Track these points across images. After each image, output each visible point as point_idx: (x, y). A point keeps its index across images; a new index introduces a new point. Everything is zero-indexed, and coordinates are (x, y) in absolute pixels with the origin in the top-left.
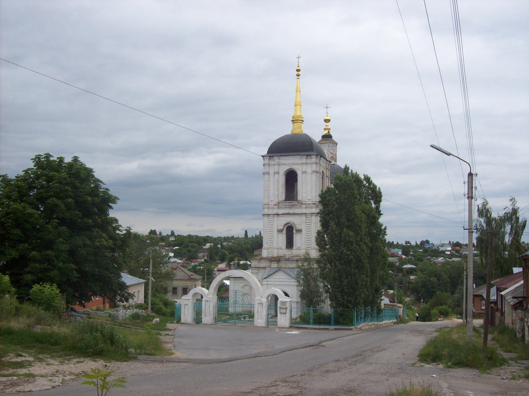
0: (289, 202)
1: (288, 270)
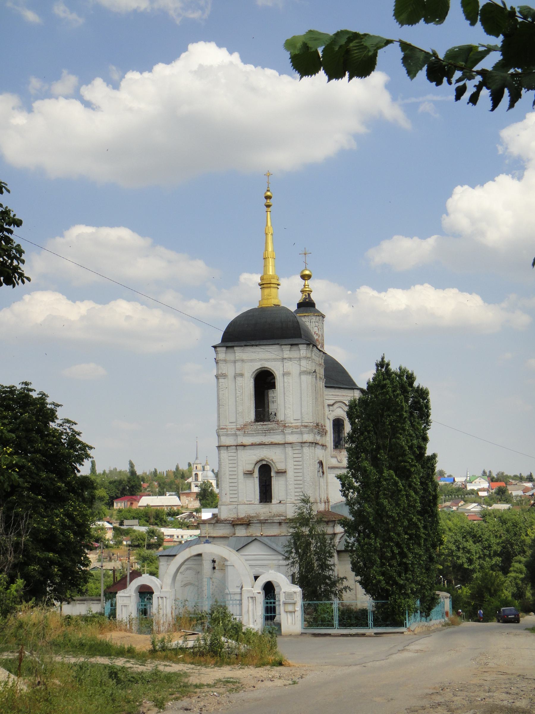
0: (262, 423)
1: (267, 541)
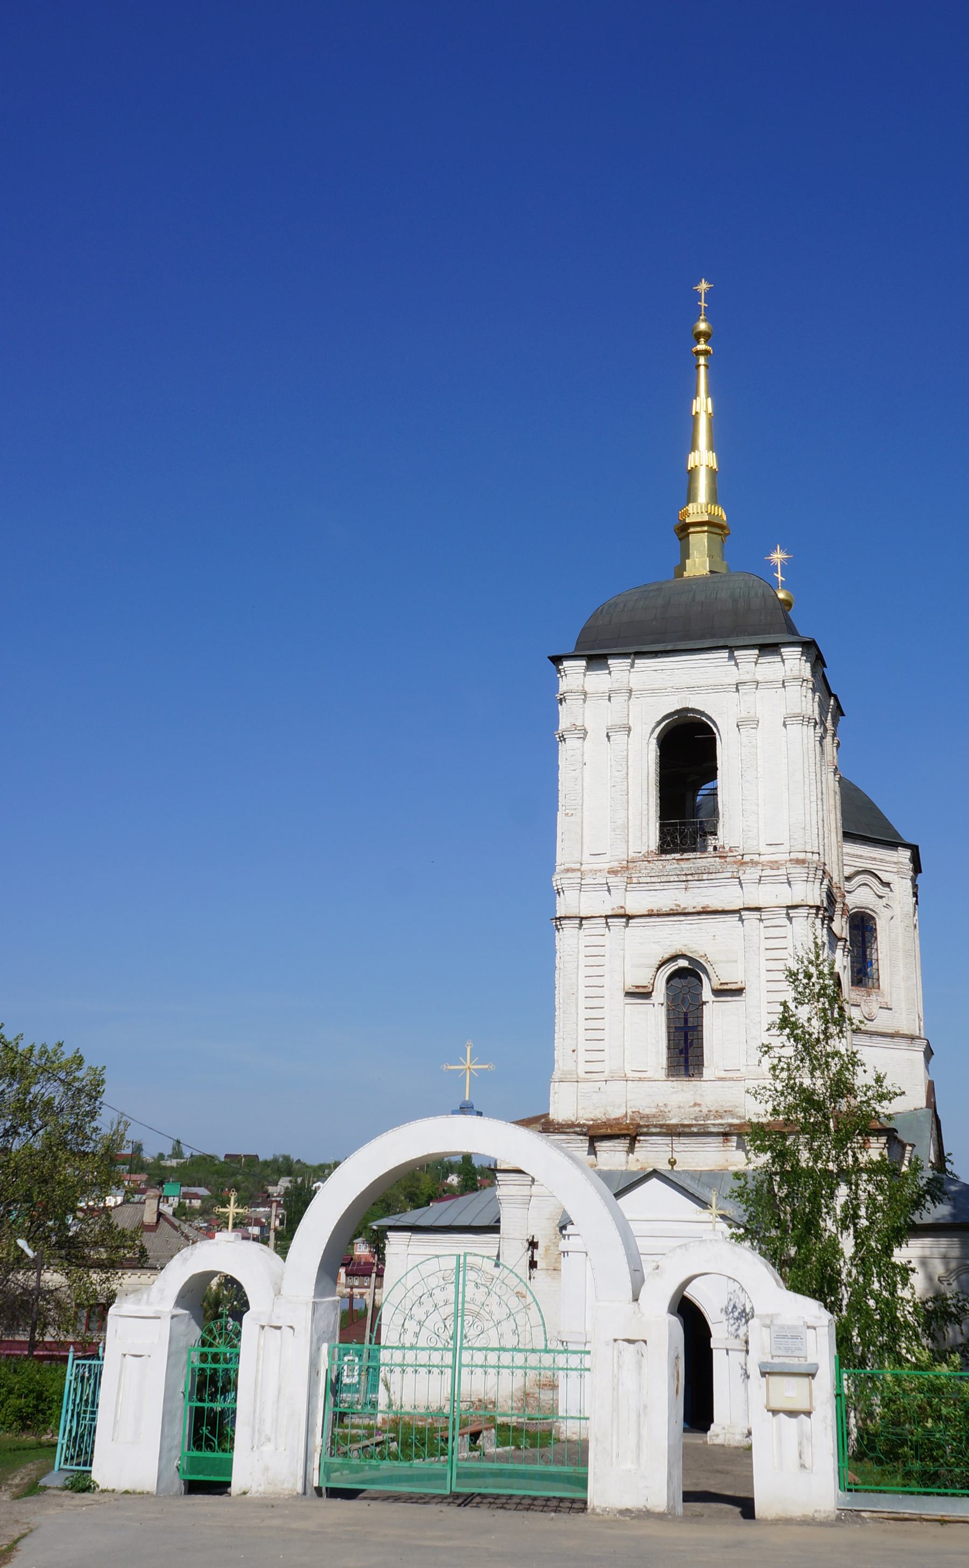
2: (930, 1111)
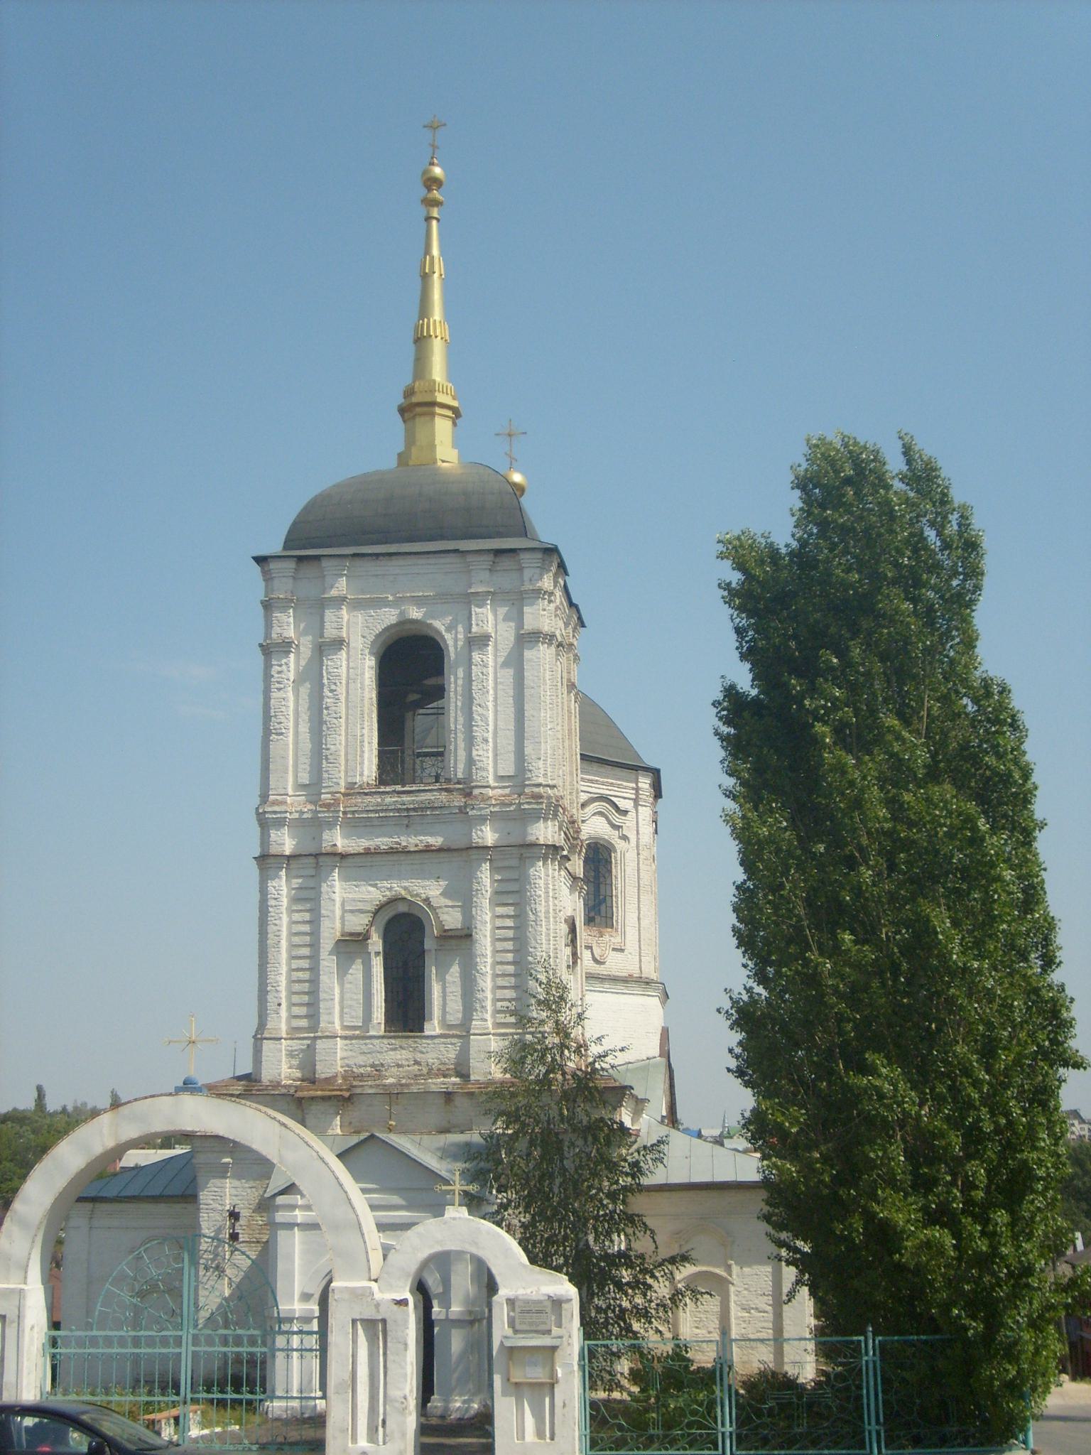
0: (399, 788)
2: (664, 1060)
